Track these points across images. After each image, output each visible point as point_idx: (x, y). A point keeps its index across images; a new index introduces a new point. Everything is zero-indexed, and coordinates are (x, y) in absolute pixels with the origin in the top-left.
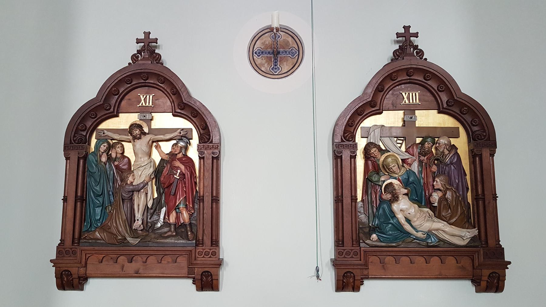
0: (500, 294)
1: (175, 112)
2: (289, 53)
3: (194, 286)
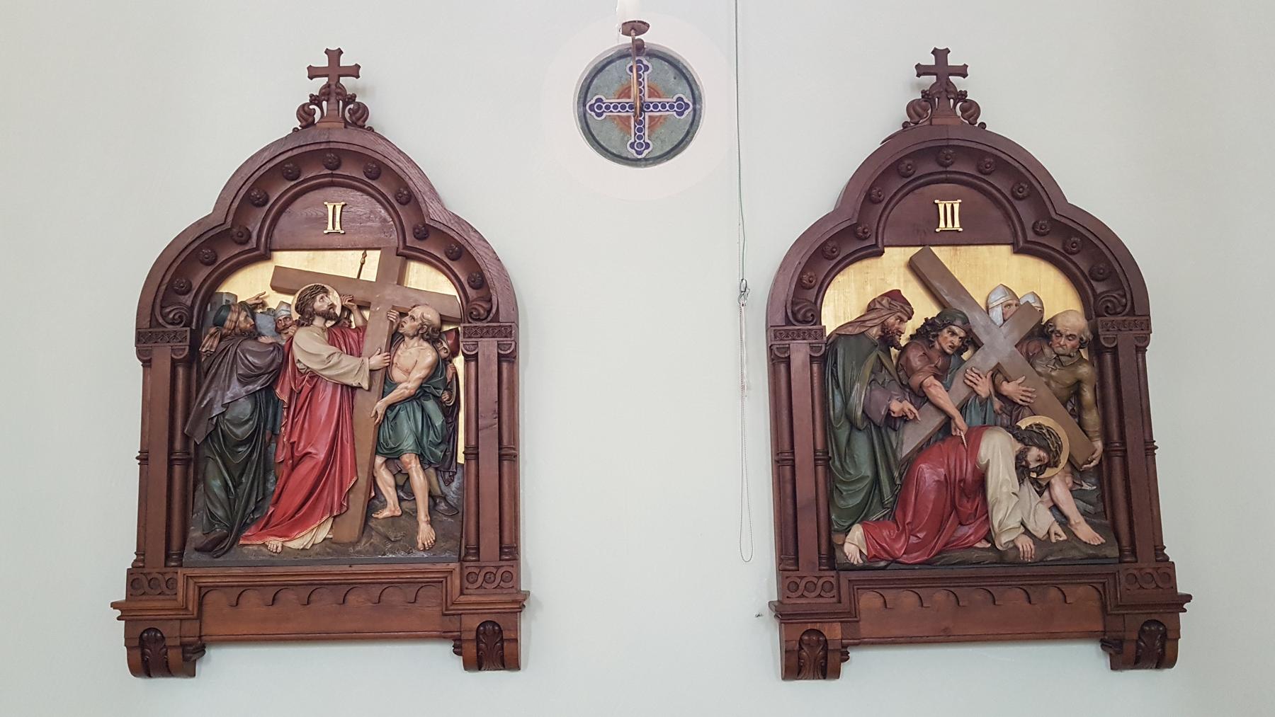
0: (1166, 672)
1: (406, 247)
2: (672, 107)
3: (459, 661)
